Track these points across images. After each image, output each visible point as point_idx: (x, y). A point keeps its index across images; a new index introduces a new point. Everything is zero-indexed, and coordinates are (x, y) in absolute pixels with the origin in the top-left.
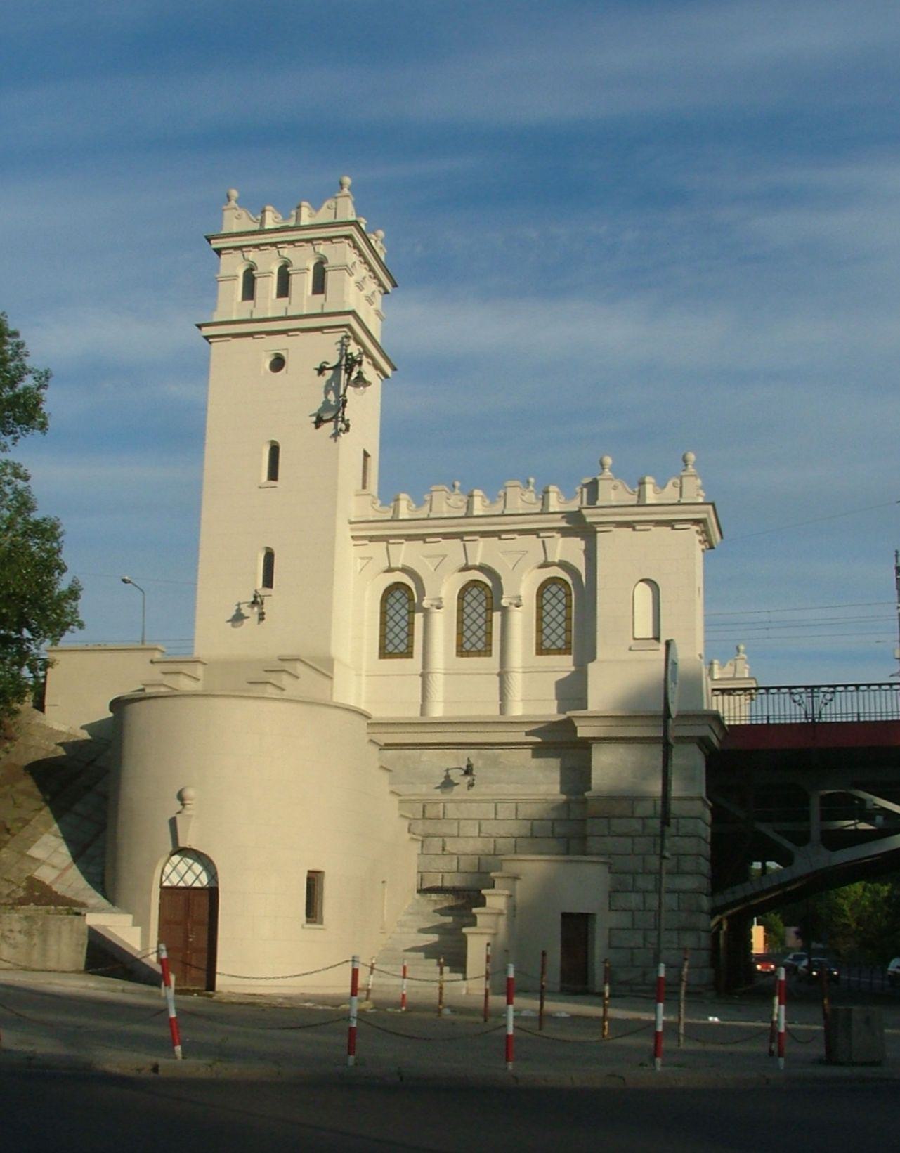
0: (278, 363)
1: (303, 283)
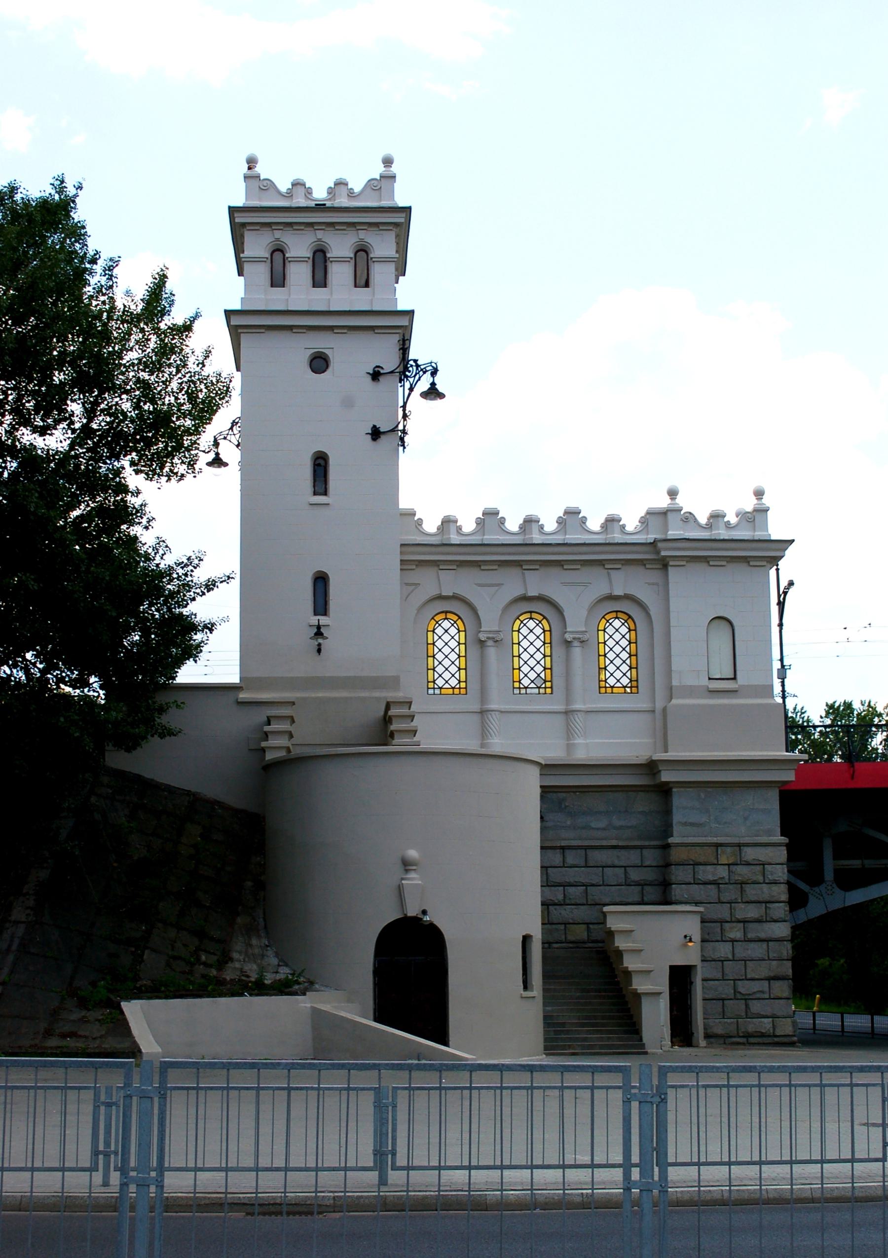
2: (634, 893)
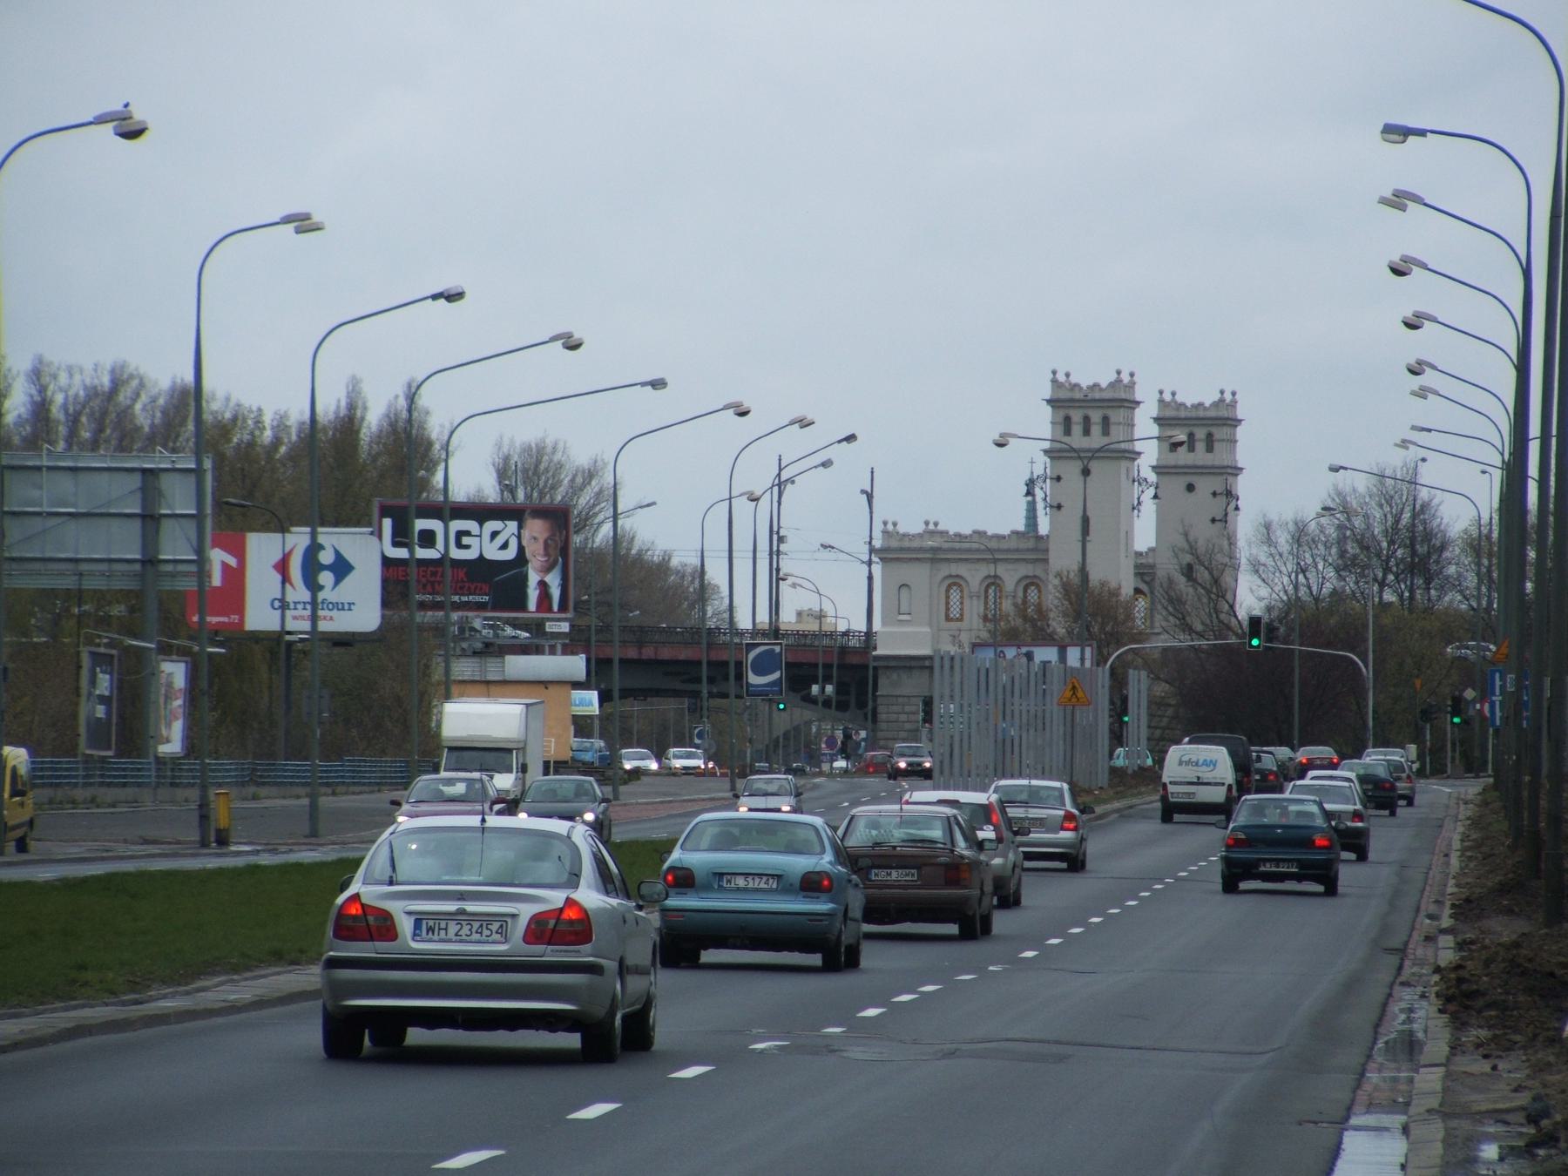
0: (1190, 488)
1: (1096, 430)
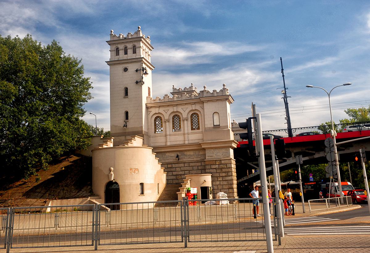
0: (126, 70)
1: (130, 51)
2: (200, 172)
